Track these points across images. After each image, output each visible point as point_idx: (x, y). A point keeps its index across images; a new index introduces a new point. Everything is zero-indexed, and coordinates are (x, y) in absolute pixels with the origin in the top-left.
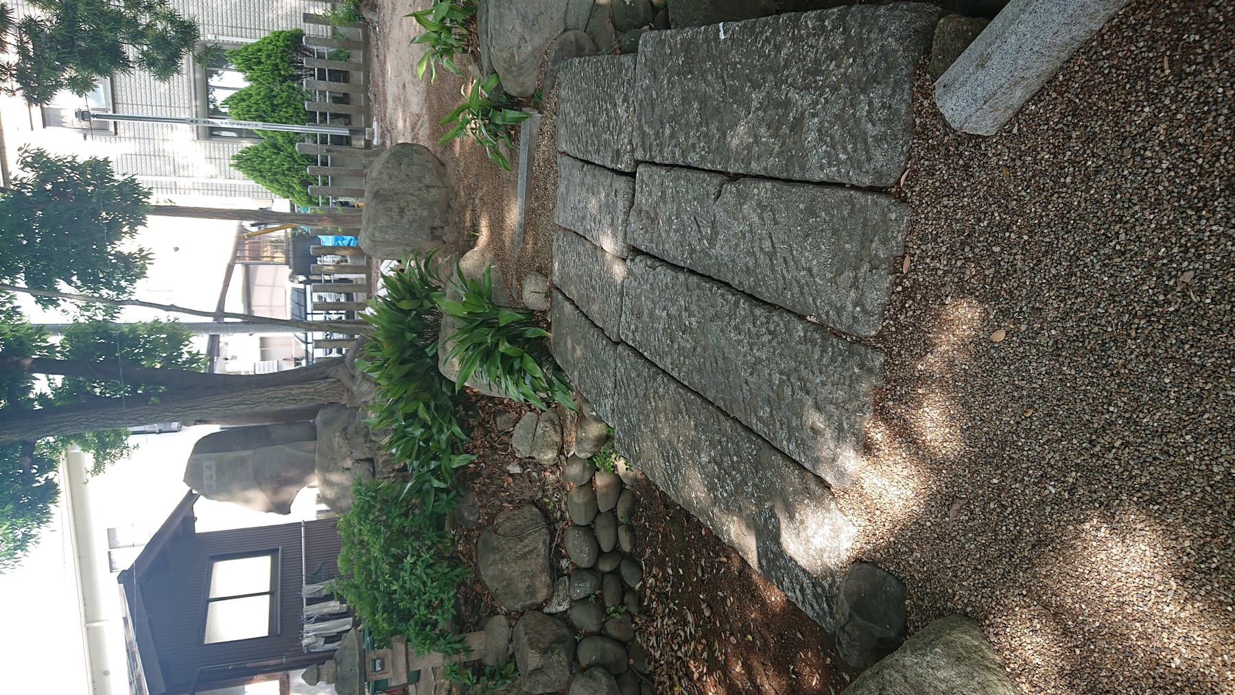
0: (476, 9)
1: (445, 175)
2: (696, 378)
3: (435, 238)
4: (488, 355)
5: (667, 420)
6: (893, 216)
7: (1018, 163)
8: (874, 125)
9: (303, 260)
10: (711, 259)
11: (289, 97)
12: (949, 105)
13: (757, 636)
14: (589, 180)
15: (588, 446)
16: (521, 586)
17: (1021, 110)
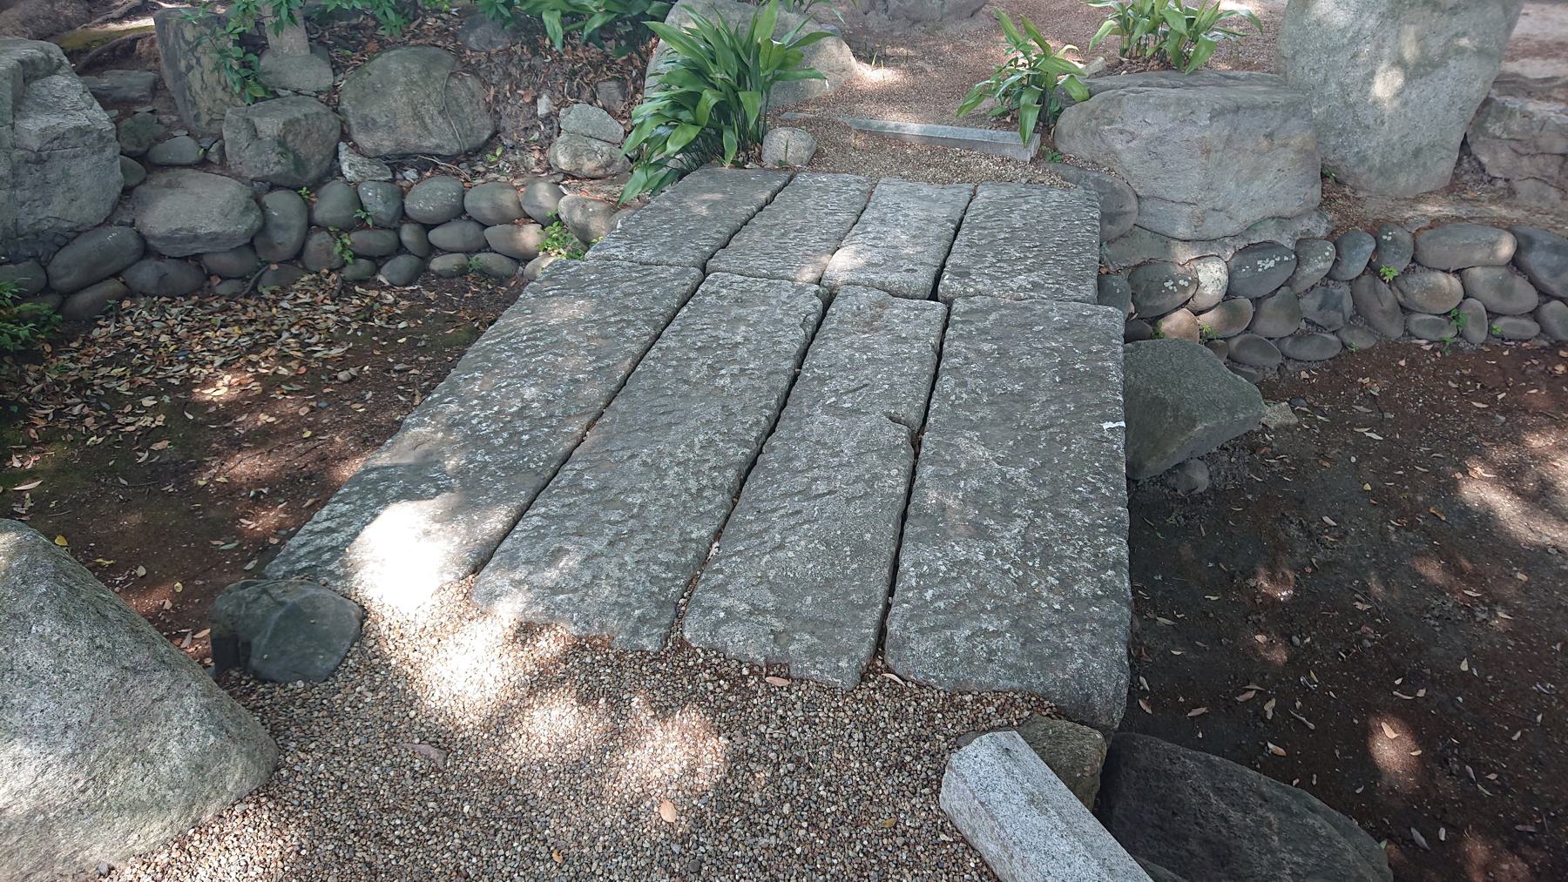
0: (1178, 70)
1: (959, 18)
2: (646, 384)
4: (698, 72)
5: (589, 338)
6: (843, 664)
7: (900, 841)
8: (967, 639)
10: (810, 407)
12: (983, 753)
13: (310, 445)
14: (934, 229)
15: (578, 217)
16: (374, 111)
17: (970, 847)
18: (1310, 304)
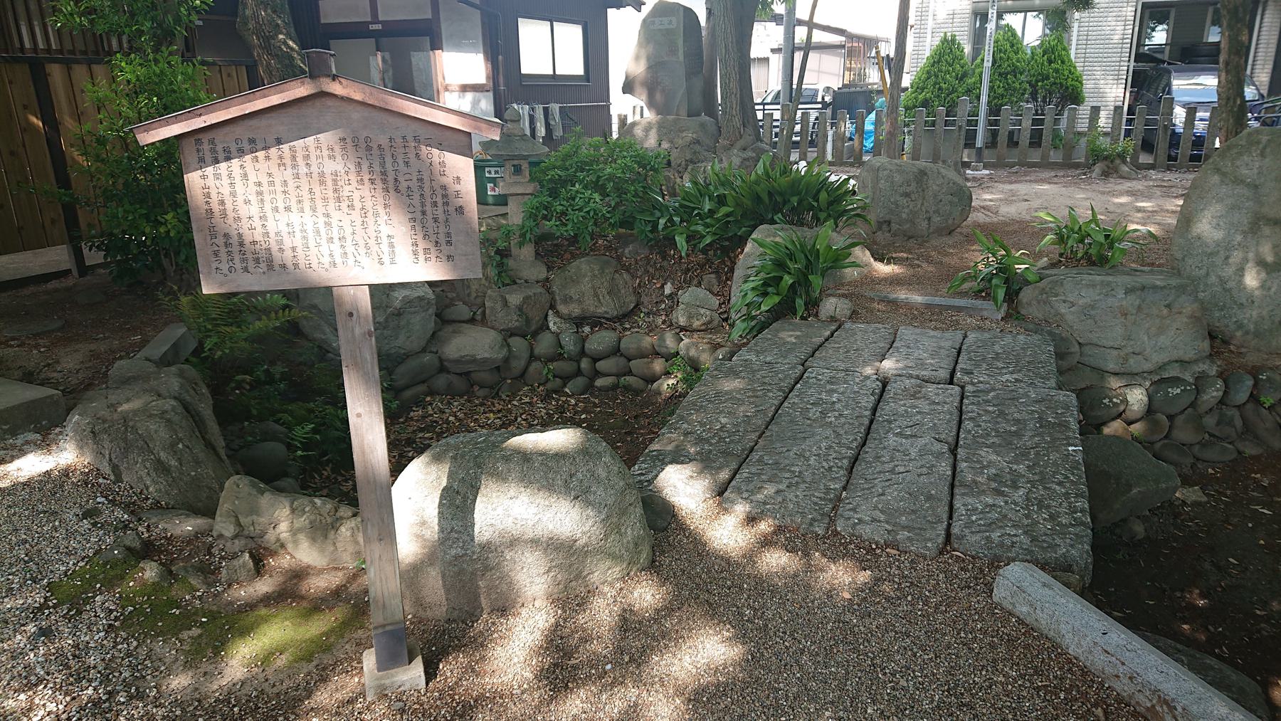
3: (880, 224)
4: (780, 265)
6: (929, 545)
9: (848, 101)
11: (1015, 89)
15: (693, 352)
16: (572, 292)
18: (1210, 421)
